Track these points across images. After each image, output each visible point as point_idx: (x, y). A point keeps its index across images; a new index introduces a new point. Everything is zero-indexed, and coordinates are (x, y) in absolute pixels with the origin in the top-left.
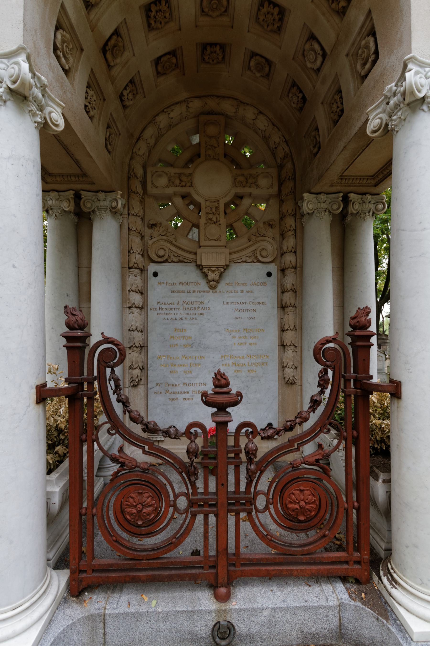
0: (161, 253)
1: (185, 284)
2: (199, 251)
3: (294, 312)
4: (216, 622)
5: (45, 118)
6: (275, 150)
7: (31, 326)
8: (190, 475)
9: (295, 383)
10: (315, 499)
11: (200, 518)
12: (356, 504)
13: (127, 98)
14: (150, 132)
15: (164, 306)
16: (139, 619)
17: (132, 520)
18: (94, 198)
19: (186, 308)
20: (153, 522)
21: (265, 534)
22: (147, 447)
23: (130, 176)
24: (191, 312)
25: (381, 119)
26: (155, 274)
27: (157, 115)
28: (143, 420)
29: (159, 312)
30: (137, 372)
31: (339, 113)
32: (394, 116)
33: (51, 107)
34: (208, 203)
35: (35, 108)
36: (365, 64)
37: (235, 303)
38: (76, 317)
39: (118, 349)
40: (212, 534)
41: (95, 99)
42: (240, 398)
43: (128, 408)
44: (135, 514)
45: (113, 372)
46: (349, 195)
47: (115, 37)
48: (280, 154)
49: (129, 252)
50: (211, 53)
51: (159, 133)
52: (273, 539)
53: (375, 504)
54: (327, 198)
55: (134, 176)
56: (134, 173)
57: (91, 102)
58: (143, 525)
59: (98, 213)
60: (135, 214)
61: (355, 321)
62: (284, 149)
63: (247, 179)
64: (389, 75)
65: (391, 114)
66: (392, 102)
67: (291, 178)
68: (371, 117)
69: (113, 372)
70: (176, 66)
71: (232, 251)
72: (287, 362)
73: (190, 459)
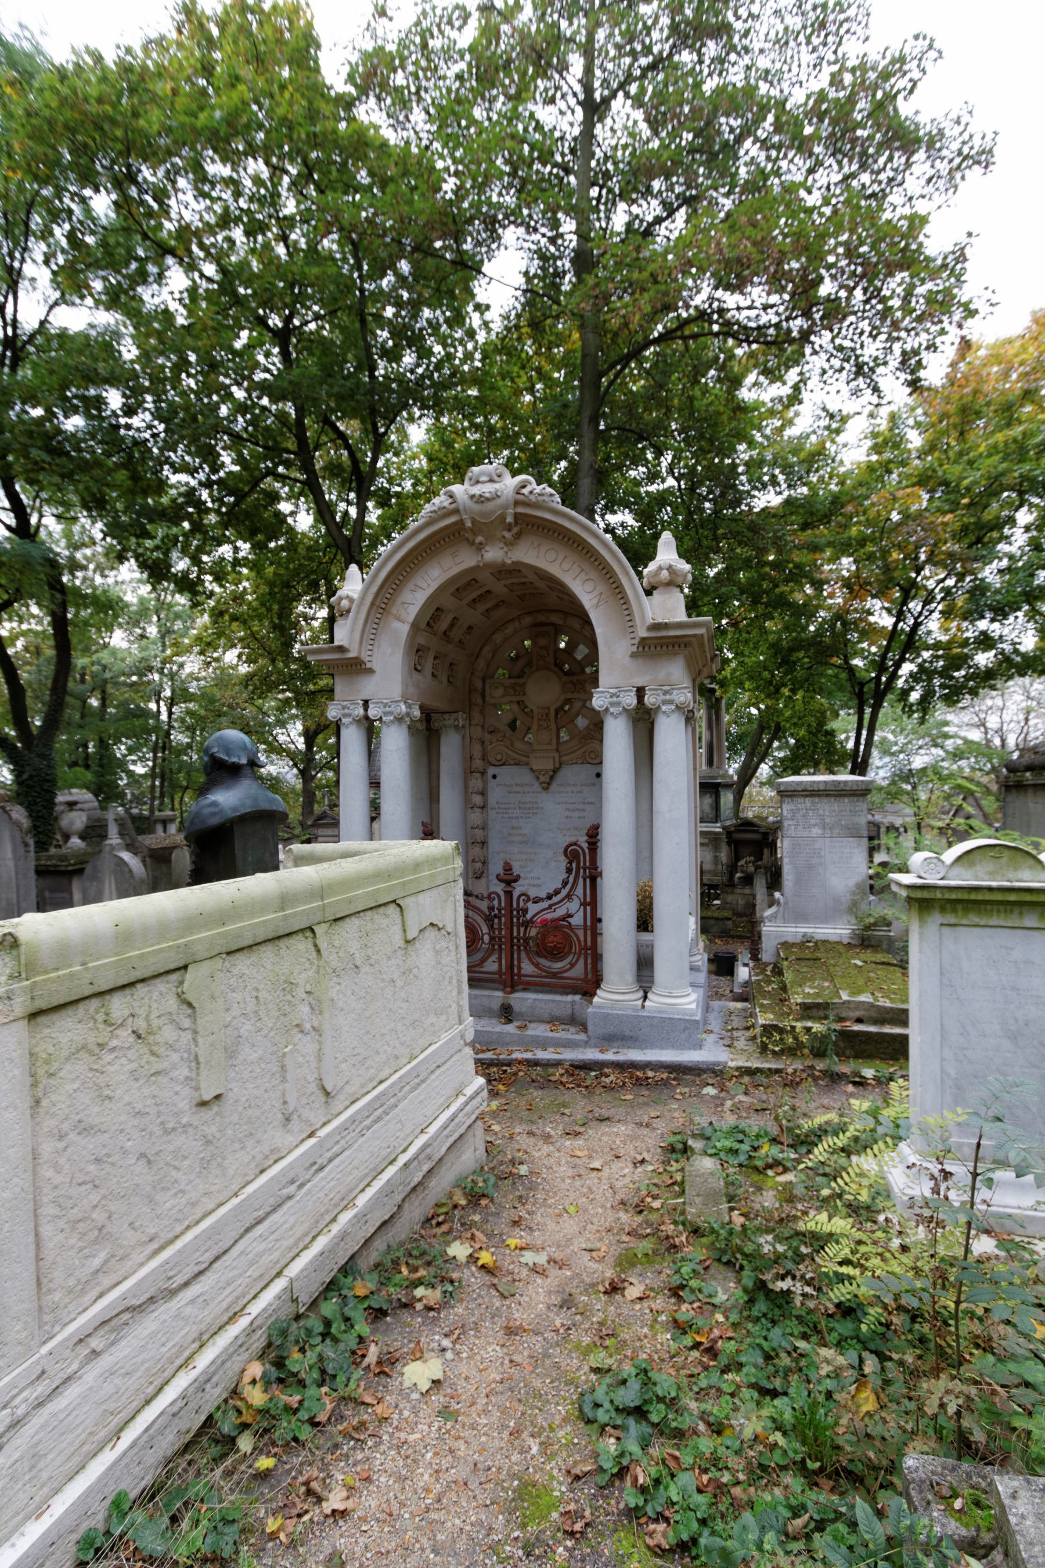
14: (487, 650)
30: (479, 865)
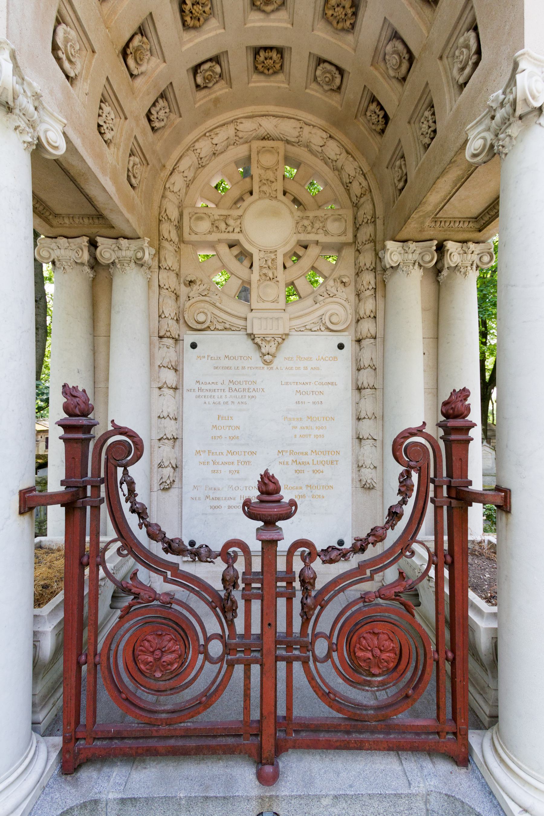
0: (201, 318)
1: (232, 358)
2: (250, 316)
3: (374, 396)
4: (258, 813)
5: (38, 138)
6: (349, 185)
7: (13, 411)
8: (225, 612)
9: (373, 488)
10: (394, 646)
11: (239, 669)
12: (450, 655)
13: (157, 118)
15: (204, 387)
16: (153, 808)
17: (148, 671)
18: (114, 246)
19: (233, 389)
20: (176, 674)
21: (327, 691)
22: (169, 573)
23: (161, 218)
24: (240, 394)
25: (484, 139)
26: (194, 346)
27: (197, 140)
28: (165, 536)
29: (198, 394)
30: (168, 471)
31: (430, 134)
32: (502, 133)
33: (47, 123)
34: (262, 254)
35: (23, 123)
36: (463, 69)
37: (297, 383)
38: (78, 399)
39: (133, 442)
40: (255, 693)
41: (113, 117)
42: (293, 508)
43: (145, 521)
44: (151, 664)
45: (126, 472)
46: (445, 243)
47: (138, 38)
48: (356, 189)
49: (160, 316)
50: (266, 59)
51: (199, 164)
52: (337, 698)
53: (476, 654)
54: (416, 247)
55: (166, 218)
56: (167, 215)
57: (107, 121)
58: (163, 679)
59: (119, 266)
60: (168, 268)
61: (448, 407)
62: (360, 184)
63: (312, 223)
64: (494, 81)
65: (498, 131)
66: (498, 117)
67: (369, 221)
68: (471, 136)
69: (126, 472)
70: (220, 76)
71: (292, 316)
72: (364, 460)
73: (227, 590)
